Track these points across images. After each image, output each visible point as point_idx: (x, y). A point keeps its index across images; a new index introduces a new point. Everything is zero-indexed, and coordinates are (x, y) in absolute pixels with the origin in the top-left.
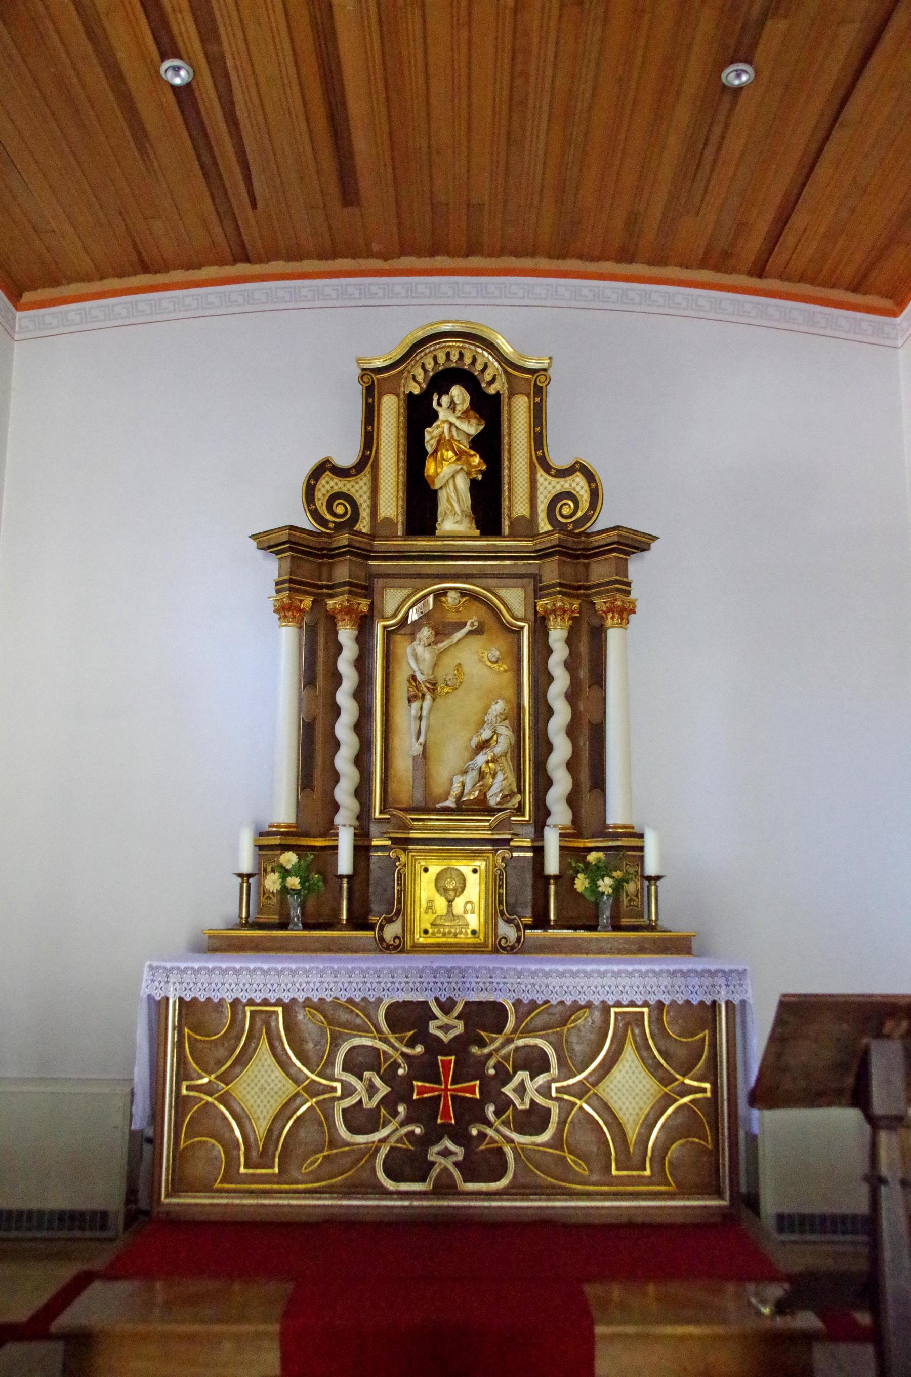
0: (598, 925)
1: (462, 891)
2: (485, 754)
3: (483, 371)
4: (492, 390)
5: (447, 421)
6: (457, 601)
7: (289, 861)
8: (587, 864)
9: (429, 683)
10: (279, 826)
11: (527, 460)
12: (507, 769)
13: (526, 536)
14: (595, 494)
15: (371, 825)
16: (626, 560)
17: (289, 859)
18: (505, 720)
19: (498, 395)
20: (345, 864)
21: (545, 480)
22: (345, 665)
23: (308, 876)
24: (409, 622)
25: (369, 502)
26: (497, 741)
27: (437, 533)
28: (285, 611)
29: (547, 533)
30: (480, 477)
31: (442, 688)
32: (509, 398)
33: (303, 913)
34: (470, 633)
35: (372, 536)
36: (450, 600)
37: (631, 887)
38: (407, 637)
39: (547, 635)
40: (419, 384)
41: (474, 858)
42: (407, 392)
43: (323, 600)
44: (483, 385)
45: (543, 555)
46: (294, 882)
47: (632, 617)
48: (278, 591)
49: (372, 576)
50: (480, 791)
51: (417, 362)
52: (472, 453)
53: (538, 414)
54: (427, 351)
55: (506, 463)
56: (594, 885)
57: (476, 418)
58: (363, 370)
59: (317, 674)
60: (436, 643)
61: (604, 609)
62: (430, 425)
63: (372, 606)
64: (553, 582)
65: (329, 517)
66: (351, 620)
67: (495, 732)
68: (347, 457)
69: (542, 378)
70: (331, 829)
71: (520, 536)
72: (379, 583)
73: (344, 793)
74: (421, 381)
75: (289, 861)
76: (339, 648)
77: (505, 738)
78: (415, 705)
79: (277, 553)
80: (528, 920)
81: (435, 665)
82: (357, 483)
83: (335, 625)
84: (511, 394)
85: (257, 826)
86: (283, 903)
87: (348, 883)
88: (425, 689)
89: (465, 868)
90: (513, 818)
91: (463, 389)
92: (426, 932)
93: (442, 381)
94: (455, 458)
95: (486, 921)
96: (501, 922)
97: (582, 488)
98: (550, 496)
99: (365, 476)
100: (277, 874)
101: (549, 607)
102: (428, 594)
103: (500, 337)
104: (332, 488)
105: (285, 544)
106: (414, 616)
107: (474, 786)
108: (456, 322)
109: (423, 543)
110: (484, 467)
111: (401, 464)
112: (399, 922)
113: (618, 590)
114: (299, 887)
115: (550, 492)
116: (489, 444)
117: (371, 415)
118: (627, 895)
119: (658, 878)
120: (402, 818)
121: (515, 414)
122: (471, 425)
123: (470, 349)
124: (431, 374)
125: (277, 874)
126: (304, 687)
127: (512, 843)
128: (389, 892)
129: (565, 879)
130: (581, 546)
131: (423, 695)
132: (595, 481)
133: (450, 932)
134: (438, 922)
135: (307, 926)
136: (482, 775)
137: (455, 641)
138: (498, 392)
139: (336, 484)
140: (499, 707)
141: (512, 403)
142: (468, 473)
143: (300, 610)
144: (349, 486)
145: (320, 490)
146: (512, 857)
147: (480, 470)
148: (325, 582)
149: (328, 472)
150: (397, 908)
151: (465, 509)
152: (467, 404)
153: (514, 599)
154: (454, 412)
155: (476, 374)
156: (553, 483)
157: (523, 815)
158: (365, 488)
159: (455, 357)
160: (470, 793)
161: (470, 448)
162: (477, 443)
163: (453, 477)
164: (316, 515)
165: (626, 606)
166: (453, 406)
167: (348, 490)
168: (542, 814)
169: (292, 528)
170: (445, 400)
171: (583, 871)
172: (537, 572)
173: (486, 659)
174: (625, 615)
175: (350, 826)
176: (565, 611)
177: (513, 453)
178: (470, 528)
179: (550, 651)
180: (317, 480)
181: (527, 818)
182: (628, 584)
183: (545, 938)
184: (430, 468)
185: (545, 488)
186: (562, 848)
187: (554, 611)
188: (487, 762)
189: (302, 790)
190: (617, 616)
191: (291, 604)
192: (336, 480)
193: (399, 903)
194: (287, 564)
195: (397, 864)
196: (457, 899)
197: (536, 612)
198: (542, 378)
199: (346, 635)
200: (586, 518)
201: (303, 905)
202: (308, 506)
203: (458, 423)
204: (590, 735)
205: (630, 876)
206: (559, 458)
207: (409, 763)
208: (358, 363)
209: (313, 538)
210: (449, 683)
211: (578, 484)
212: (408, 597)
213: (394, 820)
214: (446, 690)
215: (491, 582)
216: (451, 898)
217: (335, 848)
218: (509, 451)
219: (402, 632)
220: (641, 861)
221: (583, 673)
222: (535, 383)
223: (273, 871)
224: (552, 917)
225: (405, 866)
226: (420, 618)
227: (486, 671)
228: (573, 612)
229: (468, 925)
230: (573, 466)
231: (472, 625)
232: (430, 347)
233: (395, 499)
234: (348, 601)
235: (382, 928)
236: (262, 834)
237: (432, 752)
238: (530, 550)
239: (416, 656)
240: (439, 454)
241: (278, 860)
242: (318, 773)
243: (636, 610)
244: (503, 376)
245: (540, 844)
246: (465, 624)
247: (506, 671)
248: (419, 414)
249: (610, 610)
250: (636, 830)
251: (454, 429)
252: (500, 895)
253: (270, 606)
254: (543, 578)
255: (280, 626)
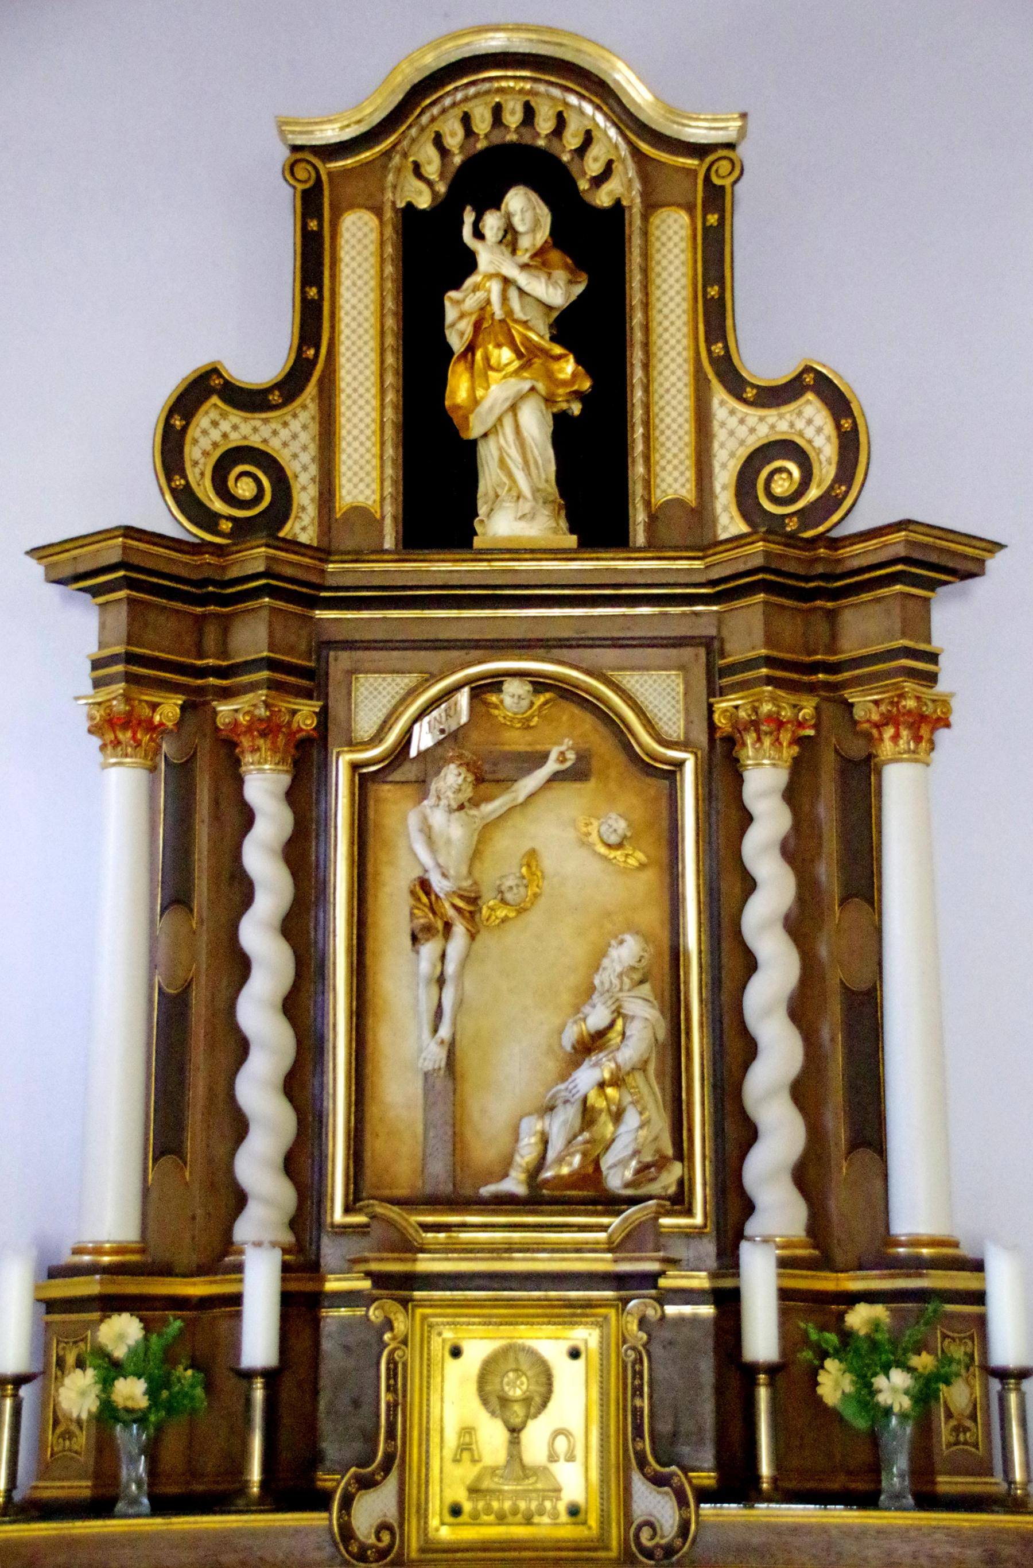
0: (878, 1492)
1: (544, 1404)
2: (596, 1065)
3: (581, 151)
4: (603, 199)
5: (497, 275)
6: (525, 703)
7: (121, 1337)
8: (846, 1336)
9: (461, 897)
10: (98, 1251)
11: (689, 367)
12: (649, 1101)
13: (687, 548)
14: (850, 445)
15: (325, 1241)
16: (927, 600)
17: (122, 1332)
18: (642, 982)
19: (618, 209)
20: (258, 1342)
21: (732, 412)
22: (261, 857)
23: (169, 1374)
24: (413, 753)
25: (313, 470)
26: (624, 1034)
27: (477, 542)
28: (115, 728)
29: (737, 540)
30: (576, 409)
31: (492, 909)
32: (645, 218)
33: (152, 1471)
34: (556, 777)
35: (323, 552)
36: (508, 701)
37: (958, 1395)
38: (409, 790)
39: (739, 780)
40: (430, 183)
41: (571, 1322)
42: (401, 205)
43: (208, 703)
44: (583, 185)
45: (727, 591)
46: (131, 1391)
47: (942, 735)
48: (97, 684)
49: (326, 645)
50: (585, 1154)
51: (423, 129)
52: (558, 350)
53: (713, 254)
54: (448, 101)
55: (638, 374)
56: (866, 1387)
57: (566, 267)
58: (296, 149)
59: (193, 876)
60: (475, 802)
61: (875, 717)
62: (457, 286)
63: (323, 715)
64: (752, 654)
65: (218, 506)
66: (274, 750)
67: (618, 1012)
68: (260, 364)
69: (724, 166)
70: (226, 1253)
71: (675, 548)
72: (340, 662)
73: (258, 1165)
74: (434, 177)
75: (121, 1337)
76: (247, 817)
77: (642, 1024)
78: (429, 950)
79: (95, 592)
80: (707, 1478)
81: (476, 855)
82: (285, 424)
83: (237, 762)
84: (650, 207)
85: (43, 1247)
86: (104, 1447)
87: (267, 1387)
88: (451, 912)
89: (550, 1343)
90: (664, 1221)
91: (534, 197)
92: (456, 1511)
93: (481, 179)
94: (516, 364)
95: (604, 1481)
96: (639, 1484)
97: (819, 430)
98: (743, 453)
99: (304, 407)
100: (90, 1372)
101: (742, 714)
102: (457, 688)
103: (620, 65)
104: (225, 436)
105: (119, 572)
106: (423, 739)
107: (570, 1142)
108: (518, 28)
109: (443, 567)
110: (586, 385)
111: (390, 379)
112: (391, 1484)
113: (912, 673)
114: (143, 1403)
115: (742, 443)
116: (597, 330)
117: (314, 260)
118: (949, 1415)
119: (1023, 1374)
120: (391, 1225)
121: (658, 257)
122: (555, 284)
123: (552, 98)
124: (458, 160)
125: (90, 1372)
126: (164, 910)
127: (663, 1282)
128: (366, 1409)
129: (793, 1374)
130: (820, 569)
131: (448, 926)
132: (850, 414)
133: (515, 1512)
134: (486, 1484)
135: (162, 1506)
136: (588, 1116)
137: (521, 798)
138: (618, 203)
139: (235, 427)
140: (627, 952)
141: (652, 229)
142: (549, 400)
143: (151, 727)
144: (265, 431)
145: (195, 441)
146: (663, 1317)
147: (575, 392)
148: (211, 662)
149: (215, 399)
150: (386, 1452)
151: (542, 485)
152: (543, 235)
153: (660, 697)
154: (514, 252)
155: (566, 158)
156: (752, 421)
157: (689, 1212)
158: (304, 437)
159: (513, 118)
160: (560, 1160)
161: (553, 339)
162: (571, 328)
163: (514, 408)
164: (187, 501)
165: (927, 710)
166: (510, 237)
167: (265, 441)
168: (734, 1209)
169: (129, 532)
170: (492, 222)
171: (837, 1354)
172: (713, 632)
173: (594, 838)
174: (924, 731)
175: (274, 1245)
176: (780, 724)
177: (654, 349)
178: (555, 531)
179: (747, 819)
180: (188, 416)
181: (698, 1220)
182: (933, 657)
183: (749, 1527)
184: (459, 387)
185: (732, 433)
186: (785, 1295)
187: (755, 724)
188: (602, 1085)
189: (155, 1160)
190: (905, 733)
191: (130, 714)
192: (235, 416)
193: (391, 1435)
194: (122, 614)
195: (387, 1336)
196: (531, 1424)
197: (712, 727)
198: (724, 166)
199: (263, 786)
200: (829, 503)
201: (152, 1451)
202: (169, 479)
203: (523, 279)
204: (847, 1020)
205: (954, 1368)
206: (763, 362)
207: (416, 1088)
208: (282, 133)
209: (186, 558)
210: (509, 896)
211: (810, 422)
212: (412, 693)
213: (377, 1231)
214: (501, 913)
215: (607, 656)
216: (516, 1421)
217: (236, 1300)
218: (646, 345)
219: (397, 776)
220: (980, 1327)
221: (827, 872)
222: (707, 179)
223: (80, 1364)
224: (765, 1469)
225: (405, 1342)
226: (439, 744)
227: (595, 867)
228: (800, 725)
229: (558, 1490)
230: (799, 377)
231: (562, 758)
232: (454, 92)
233: (376, 462)
234: (267, 705)
235: (347, 1503)
236: (56, 1273)
237: (469, 1060)
238: (702, 579)
239: (430, 834)
240: (479, 355)
241: (94, 1337)
242: (195, 1119)
243: (953, 719)
244: (629, 162)
245: (727, 1283)
246: (544, 757)
247: (642, 866)
248: (430, 258)
249: (888, 720)
250: (966, 1251)
251: (513, 294)
252: (637, 1412)
253: (78, 718)
254: (728, 647)
255: (105, 766)
